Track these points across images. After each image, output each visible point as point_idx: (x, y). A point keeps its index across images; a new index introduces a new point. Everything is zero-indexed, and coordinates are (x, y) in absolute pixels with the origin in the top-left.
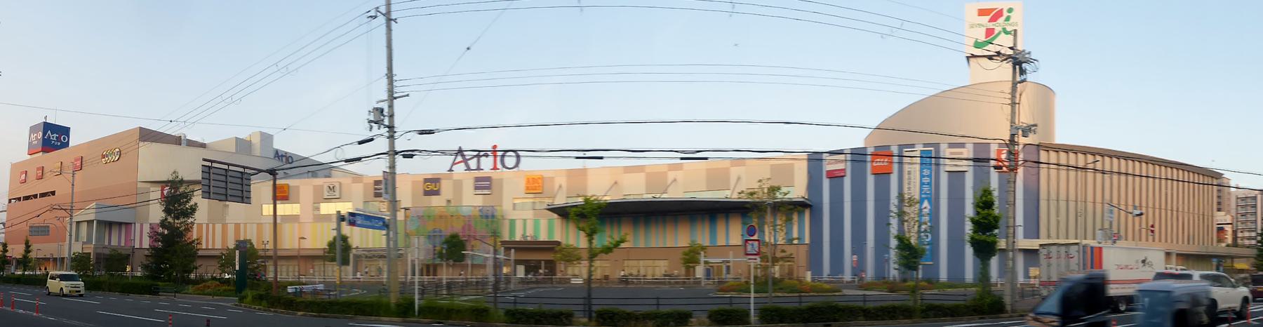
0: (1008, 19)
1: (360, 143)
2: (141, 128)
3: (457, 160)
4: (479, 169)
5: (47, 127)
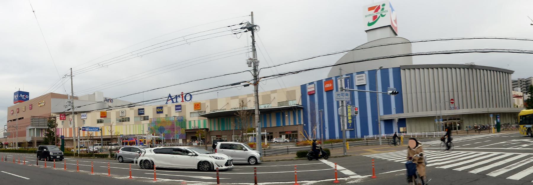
0: (383, 9)
2: (51, 93)
3: (169, 99)
4: (177, 102)
5: (20, 93)
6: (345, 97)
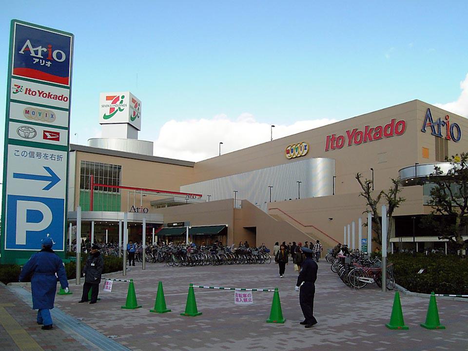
1: (101, 124)
6: (90, 176)
